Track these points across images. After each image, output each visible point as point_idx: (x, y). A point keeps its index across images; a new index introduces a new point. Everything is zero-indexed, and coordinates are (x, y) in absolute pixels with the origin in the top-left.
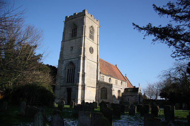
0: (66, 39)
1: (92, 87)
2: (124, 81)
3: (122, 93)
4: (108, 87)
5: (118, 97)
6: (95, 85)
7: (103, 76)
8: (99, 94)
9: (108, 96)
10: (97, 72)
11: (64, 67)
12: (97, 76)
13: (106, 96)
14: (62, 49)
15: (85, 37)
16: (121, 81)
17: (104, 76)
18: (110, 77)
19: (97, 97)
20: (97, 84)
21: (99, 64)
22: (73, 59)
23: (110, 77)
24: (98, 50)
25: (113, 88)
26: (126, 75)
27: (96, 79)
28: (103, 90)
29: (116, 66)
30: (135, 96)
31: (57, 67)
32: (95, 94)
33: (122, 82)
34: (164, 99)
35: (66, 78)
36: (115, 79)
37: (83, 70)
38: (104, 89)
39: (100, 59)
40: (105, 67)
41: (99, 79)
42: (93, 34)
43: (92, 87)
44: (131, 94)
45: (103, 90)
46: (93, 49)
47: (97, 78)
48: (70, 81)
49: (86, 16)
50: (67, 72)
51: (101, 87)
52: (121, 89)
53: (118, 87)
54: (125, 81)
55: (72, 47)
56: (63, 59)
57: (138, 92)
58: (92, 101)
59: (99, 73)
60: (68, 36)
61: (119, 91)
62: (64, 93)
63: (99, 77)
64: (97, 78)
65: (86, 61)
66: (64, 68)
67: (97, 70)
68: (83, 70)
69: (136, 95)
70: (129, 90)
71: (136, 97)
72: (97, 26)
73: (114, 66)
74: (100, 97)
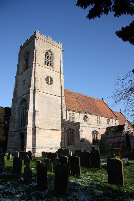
0: (20, 72)
1: (54, 130)
2: (112, 118)
3: (102, 135)
4: (75, 128)
5: (94, 140)
6: (59, 126)
7: (72, 113)
8: (65, 139)
9: (76, 139)
10: (61, 109)
11: (17, 107)
12: (62, 114)
13: (73, 140)
14: (16, 85)
15: (35, 64)
16: (106, 119)
17: (74, 113)
18: (85, 114)
19: (63, 143)
20: (62, 125)
21: (63, 98)
22: (25, 95)
23: (85, 114)
24: (62, 79)
25: (81, 128)
26: (120, 110)
27: (60, 119)
28: (69, 132)
29: (103, 100)
30: (118, 137)
31: (10, 106)
32: (61, 138)
33: (108, 120)
34: (23, 172)
35: (21, 120)
36: (96, 117)
37: (34, 108)
38: (70, 131)
39: (65, 91)
40: (72, 100)
41: (64, 118)
42: (53, 60)
43: (54, 130)
44: (113, 135)
45: (69, 132)
46: (51, 79)
47: (62, 117)
48: (23, 125)
49: (37, 38)
50: (21, 113)
51: (67, 129)
52: (99, 128)
53: (93, 126)
54: (115, 117)
55: (25, 81)
56: (18, 97)
57: (123, 131)
58: (54, 149)
59: (64, 110)
60: (21, 68)
61: (95, 133)
62: (18, 139)
63: (64, 114)
64: (62, 117)
65: (36, 94)
66: (18, 108)
67: (61, 106)
68: (34, 108)
69: (120, 136)
70: (112, 130)
71: (120, 139)
72: (58, 50)
73: (99, 101)
74: (66, 142)
